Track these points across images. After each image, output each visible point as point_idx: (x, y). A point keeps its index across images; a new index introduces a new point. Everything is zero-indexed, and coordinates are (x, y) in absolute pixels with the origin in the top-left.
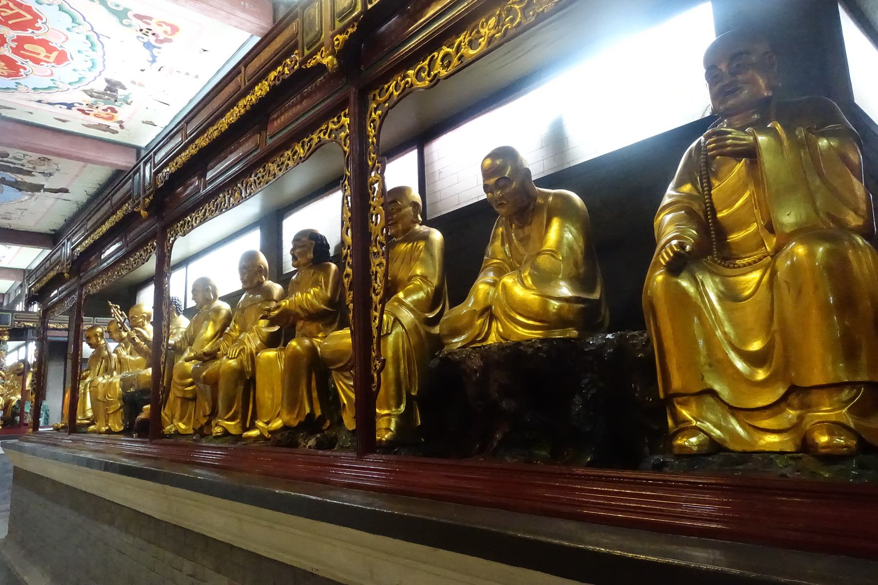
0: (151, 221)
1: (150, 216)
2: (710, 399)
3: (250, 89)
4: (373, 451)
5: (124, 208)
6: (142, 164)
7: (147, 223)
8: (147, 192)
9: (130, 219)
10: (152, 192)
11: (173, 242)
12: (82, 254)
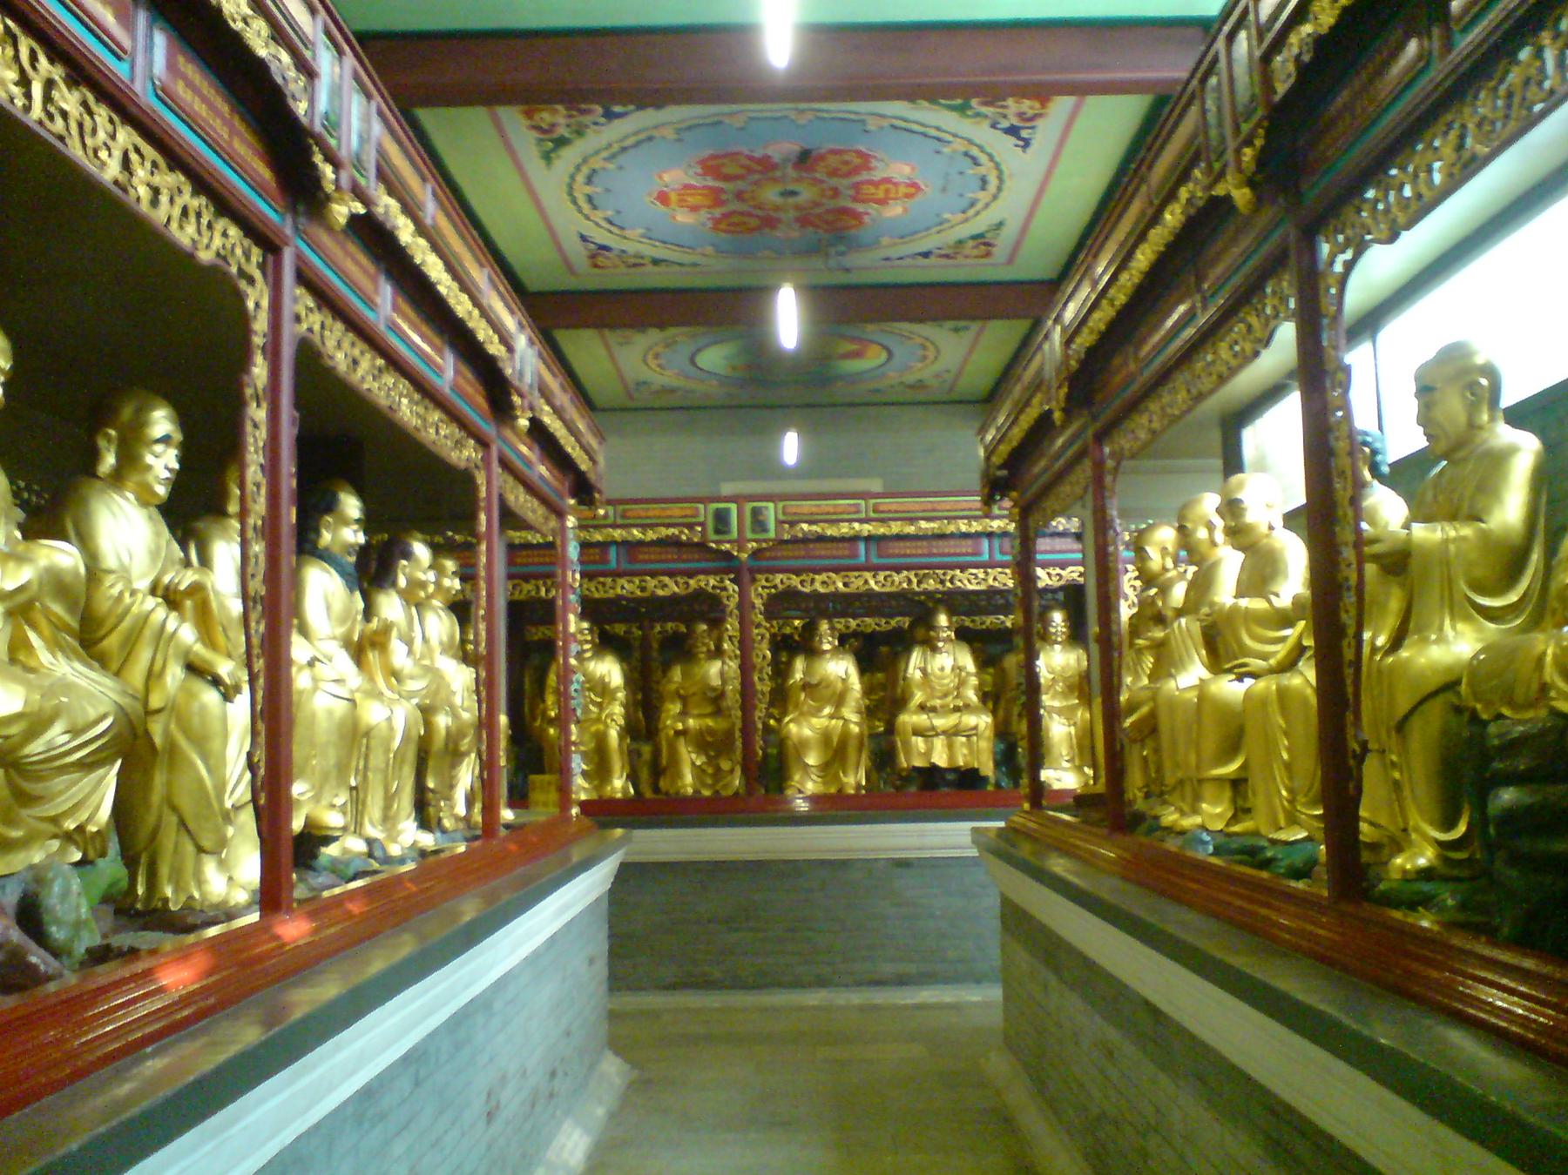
0: (1268, 214)
1: (1259, 201)
2: (533, 283)
3: (1156, 219)
4: (865, 664)
5: (1184, 193)
6: (1220, 44)
7: (1068, 433)
8: (1245, 128)
9: (1211, 217)
10: (1258, 125)
11: (1349, 266)
12: (1091, 352)
